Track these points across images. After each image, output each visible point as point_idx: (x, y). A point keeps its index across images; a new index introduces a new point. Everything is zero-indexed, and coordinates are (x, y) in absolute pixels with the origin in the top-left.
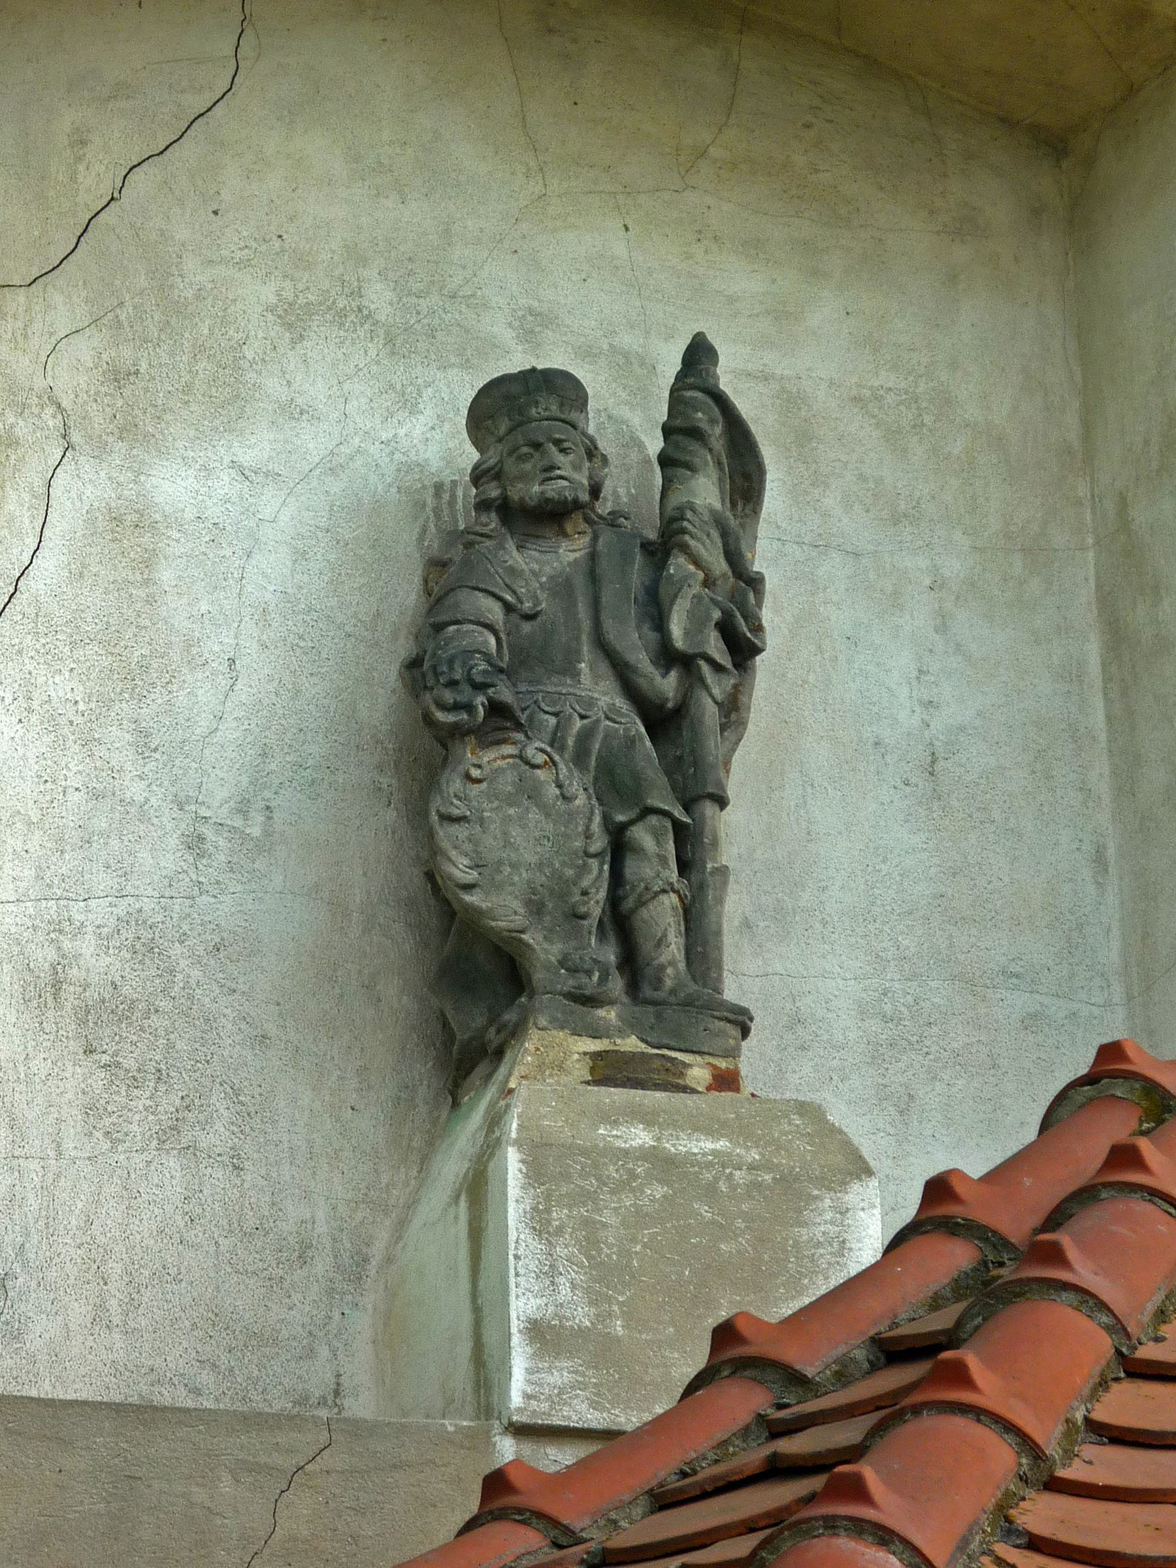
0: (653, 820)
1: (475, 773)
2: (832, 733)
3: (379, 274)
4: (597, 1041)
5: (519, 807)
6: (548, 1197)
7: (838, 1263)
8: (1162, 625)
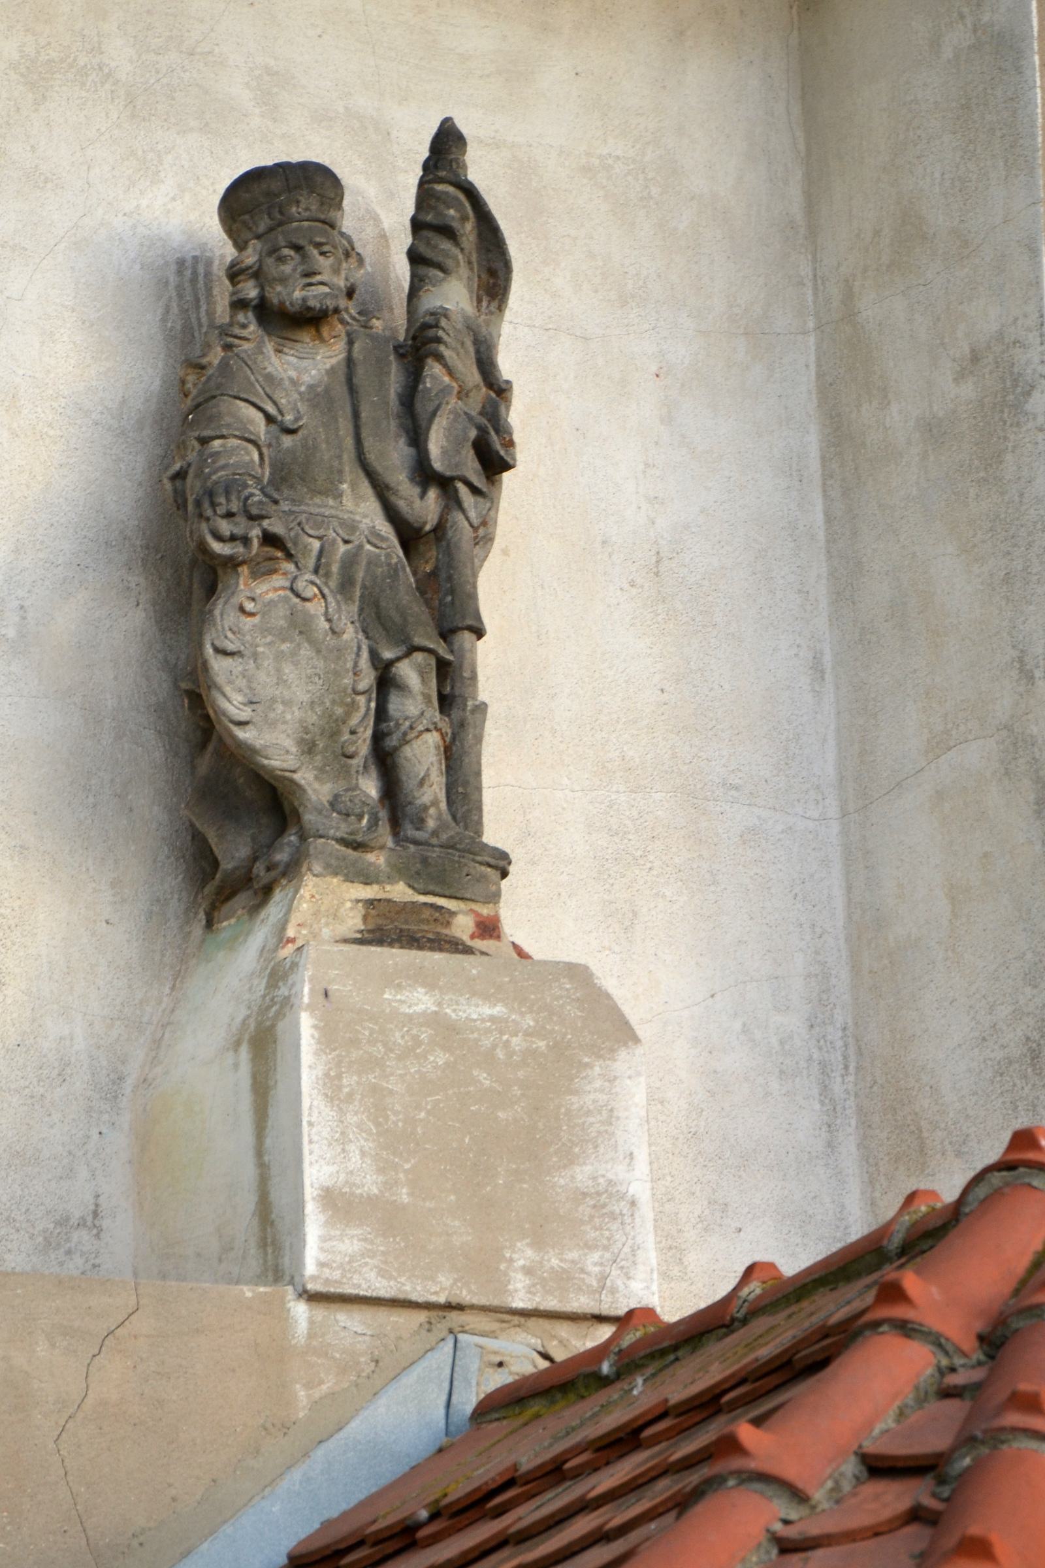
0: (419, 657)
1: (249, 606)
2: (560, 531)
3: (118, 28)
4: (368, 888)
5: (291, 642)
6: (339, 1064)
7: (606, 1131)
8: (890, 432)
